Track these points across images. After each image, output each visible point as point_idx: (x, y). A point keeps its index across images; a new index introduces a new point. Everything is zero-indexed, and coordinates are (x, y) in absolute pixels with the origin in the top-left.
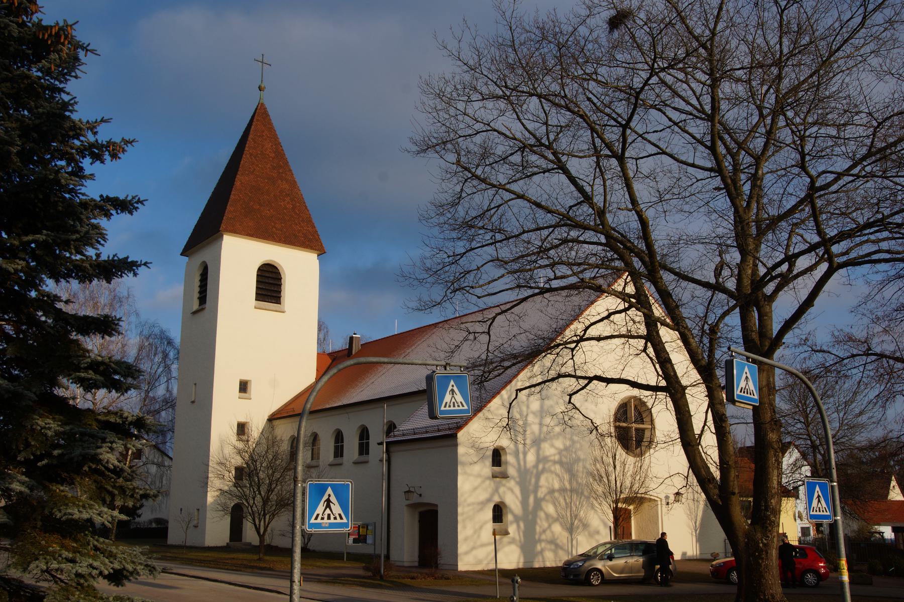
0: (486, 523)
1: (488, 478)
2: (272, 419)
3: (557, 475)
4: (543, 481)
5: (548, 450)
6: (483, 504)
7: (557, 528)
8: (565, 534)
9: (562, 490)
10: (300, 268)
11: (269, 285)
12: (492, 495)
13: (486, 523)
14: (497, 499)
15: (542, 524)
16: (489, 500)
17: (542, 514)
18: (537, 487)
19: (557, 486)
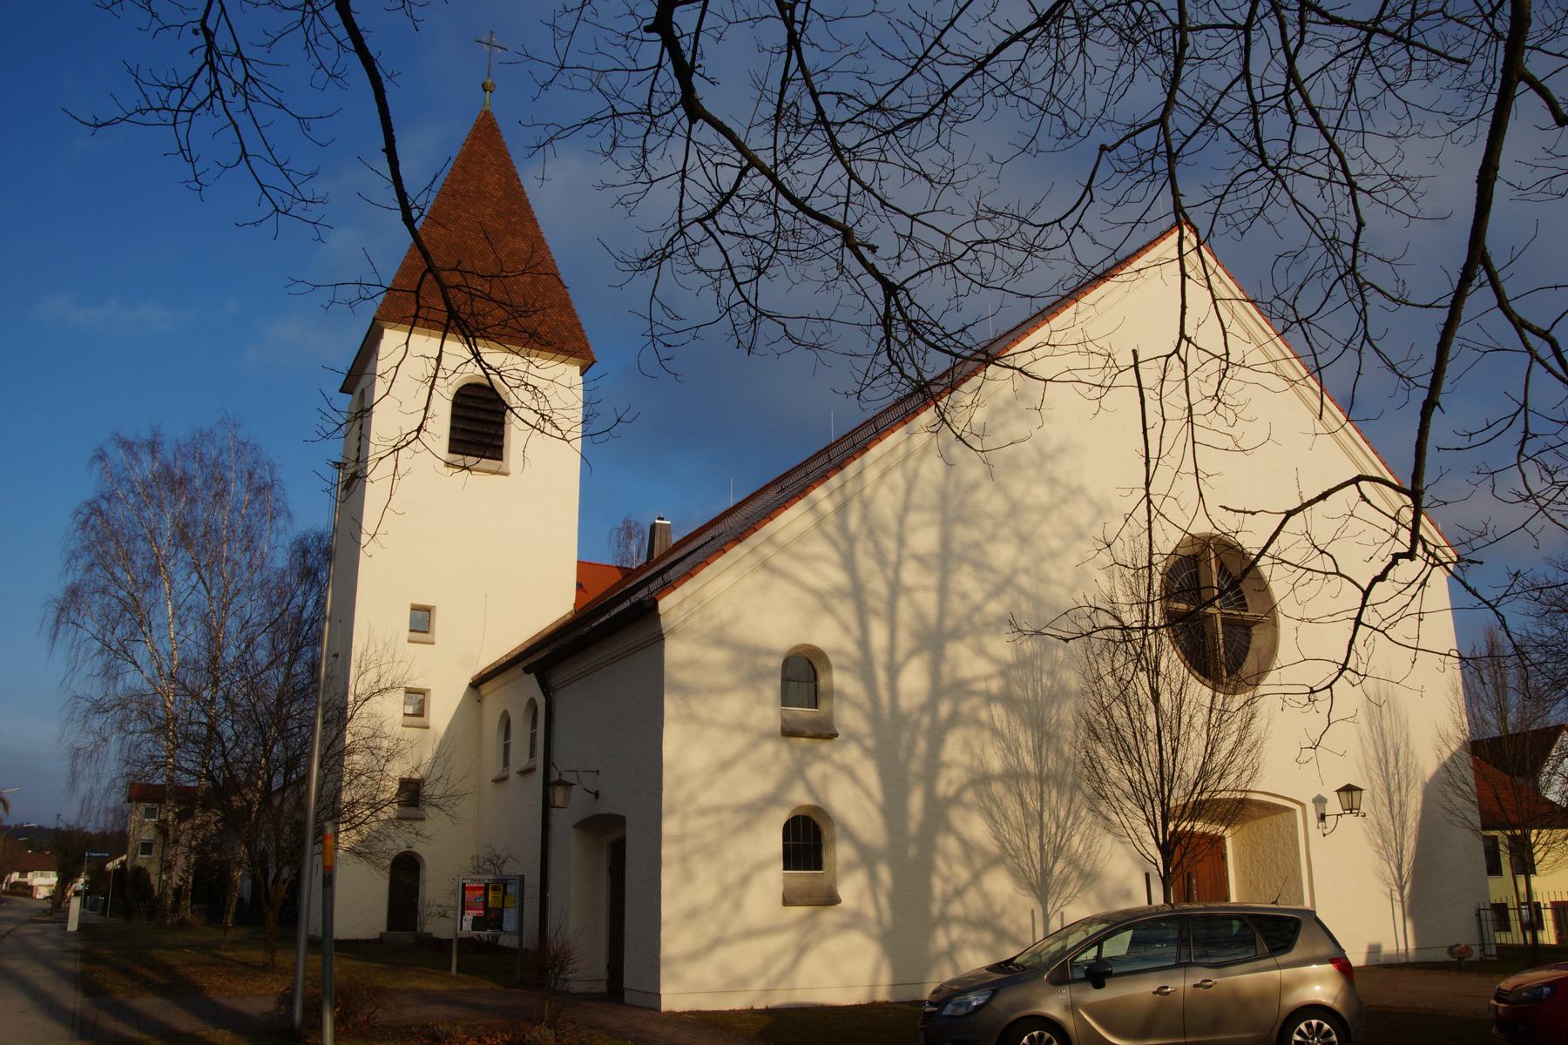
0: (761, 866)
1: (766, 736)
2: (477, 684)
3: (996, 733)
4: (953, 748)
5: (967, 662)
6: (754, 811)
7: (1000, 885)
8: (1027, 901)
9: (1013, 777)
10: (548, 388)
11: (479, 426)
12: (785, 785)
13: (761, 866)
14: (800, 797)
15: (950, 870)
16: (772, 800)
17: (951, 844)
18: (934, 765)
19: (996, 764)
